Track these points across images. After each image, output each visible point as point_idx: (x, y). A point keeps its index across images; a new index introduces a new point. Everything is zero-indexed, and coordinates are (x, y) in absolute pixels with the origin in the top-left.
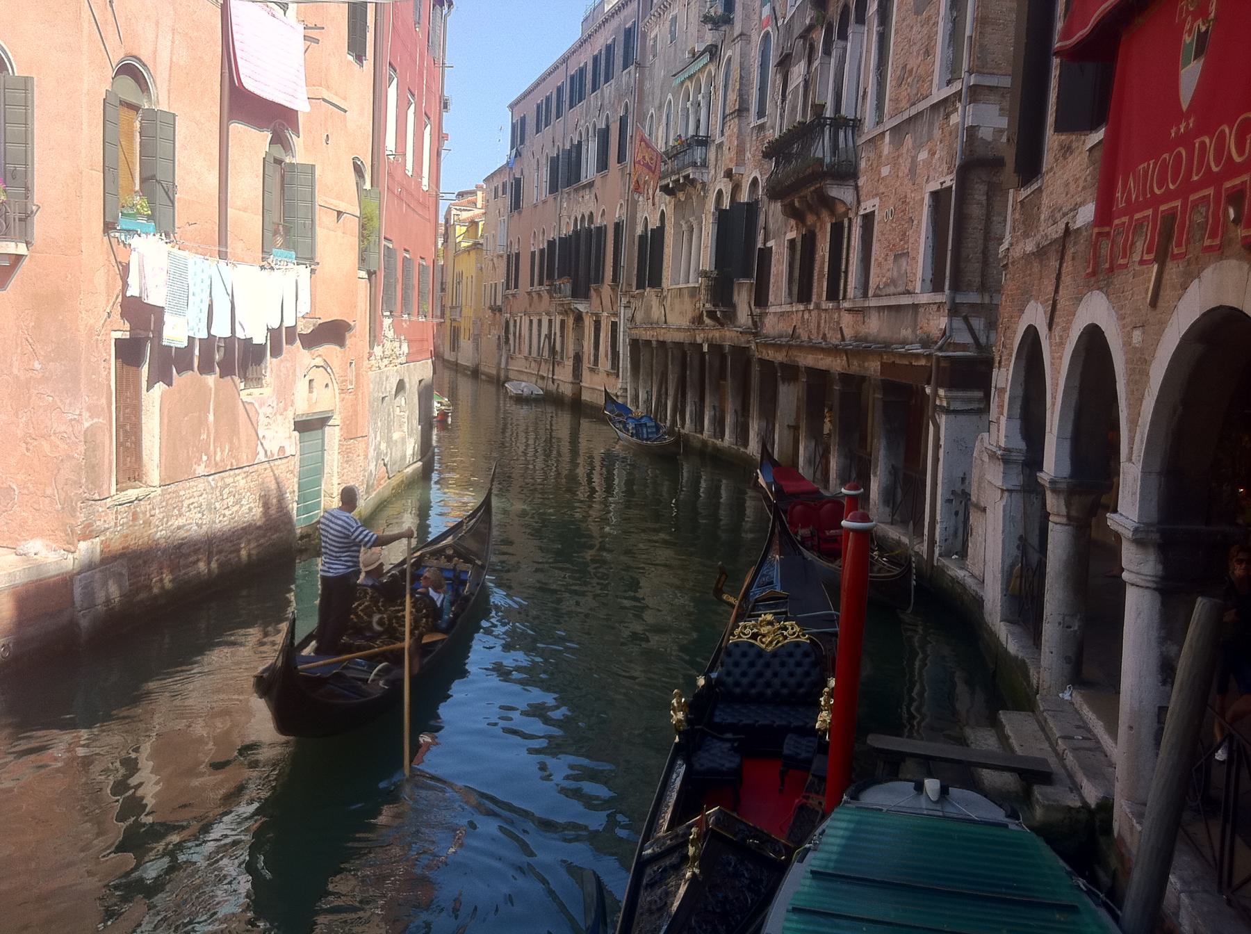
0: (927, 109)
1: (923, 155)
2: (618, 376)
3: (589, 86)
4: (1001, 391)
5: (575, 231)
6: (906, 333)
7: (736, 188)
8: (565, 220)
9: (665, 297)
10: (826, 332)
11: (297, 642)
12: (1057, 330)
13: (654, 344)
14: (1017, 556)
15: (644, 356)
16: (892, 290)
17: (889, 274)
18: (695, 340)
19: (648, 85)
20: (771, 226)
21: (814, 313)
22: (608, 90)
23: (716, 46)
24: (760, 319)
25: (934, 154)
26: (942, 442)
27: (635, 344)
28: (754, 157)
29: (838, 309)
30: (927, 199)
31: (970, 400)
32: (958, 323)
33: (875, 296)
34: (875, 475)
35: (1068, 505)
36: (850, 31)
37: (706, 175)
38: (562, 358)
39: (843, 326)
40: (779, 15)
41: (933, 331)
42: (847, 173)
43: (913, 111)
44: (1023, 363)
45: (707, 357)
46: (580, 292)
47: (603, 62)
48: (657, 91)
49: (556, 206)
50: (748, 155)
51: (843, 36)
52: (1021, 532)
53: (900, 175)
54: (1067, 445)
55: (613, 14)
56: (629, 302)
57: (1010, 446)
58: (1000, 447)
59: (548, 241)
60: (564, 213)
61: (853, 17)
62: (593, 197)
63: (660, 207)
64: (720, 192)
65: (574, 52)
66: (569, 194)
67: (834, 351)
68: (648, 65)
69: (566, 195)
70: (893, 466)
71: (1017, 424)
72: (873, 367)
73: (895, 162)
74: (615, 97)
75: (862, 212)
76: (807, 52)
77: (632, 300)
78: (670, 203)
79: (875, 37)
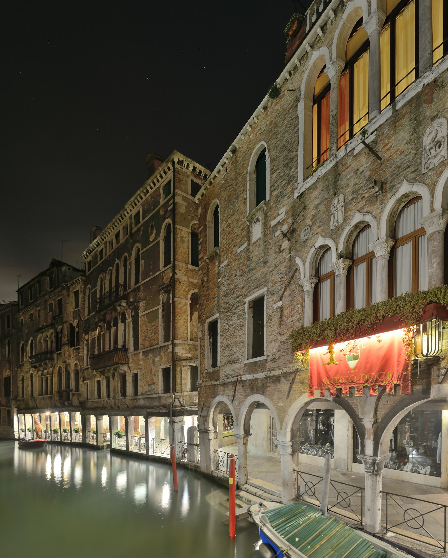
4: (93, 421)
12: (236, 403)
30: (161, 370)
32: (177, 400)
33: (141, 395)
51: (116, 325)
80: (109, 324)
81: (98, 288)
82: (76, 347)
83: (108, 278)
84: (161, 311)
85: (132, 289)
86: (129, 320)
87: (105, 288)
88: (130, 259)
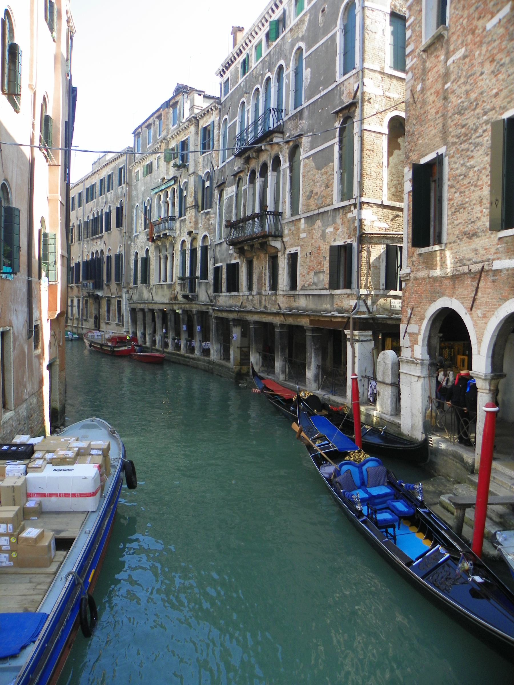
0: (331, 210)
1: (330, 230)
2: (123, 325)
3: (98, 193)
4: (414, 336)
5: (92, 259)
6: (328, 306)
7: (194, 239)
8: (85, 255)
9: (152, 289)
10: (267, 305)
11: (393, 534)
13: (146, 310)
14: (427, 405)
15: (140, 316)
16: (314, 287)
17: (311, 280)
18: (173, 308)
19: (134, 193)
20: (218, 256)
21: (257, 297)
22: (110, 195)
23: (177, 177)
24: (215, 299)
25: (338, 229)
26: (357, 355)
27: (133, 311)
28: (204, 226)
29: (276, 295)
31: (367, 336)
33: (302, 289)
34: (309, 369)
35: (490, 385)
36: (269, 174)
37: (174, 234)
38: (87, 317)
39: (279, 303)
40: (214, 165)
41: (345, 306)
42: (279, 235)
43: (321, 210)
44: (431, 322)
45: (181, 316)
46: (98, 285)
47: (106, 183)
48: (140, 196)
49: (80, 247)
50: (200, 225)
52: (428, 394)
53: (314, 237)
54: (490, 360)
55: (111, 161)
56: (128, 291)
57: (424, 358)
58: (416, 359)
59: (76, 264)
60: (85, 250)
61: (270, 168)
62: (103, 243)
63: (145, 247)
64: (184, 241)
65: (89, 177)
66: (88, 241)
67: (277, 314)
68: (133, 184)
69: (86, 242)
70: (317, 365)
71: (426, 348)
72: (305, 322)
73: (310, 232)
74: (114, 198)
75: (287, 252)
76: (236, 182)
77: (130, 290)
78: (152, 246)
79: (288, 178)
80: (253, 173)
81: (238, 119)
82: (206, 211)
83: (252, 102)
84: (336, 148)
85: (290, 115)
86: (285, 165)
87: (248, 118)
88: (287, 69)
